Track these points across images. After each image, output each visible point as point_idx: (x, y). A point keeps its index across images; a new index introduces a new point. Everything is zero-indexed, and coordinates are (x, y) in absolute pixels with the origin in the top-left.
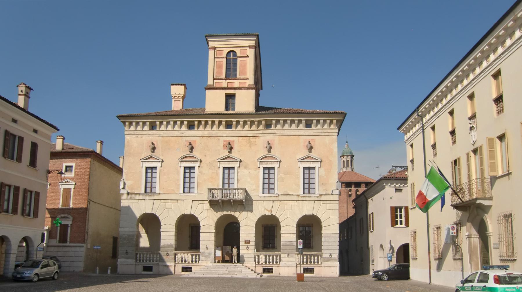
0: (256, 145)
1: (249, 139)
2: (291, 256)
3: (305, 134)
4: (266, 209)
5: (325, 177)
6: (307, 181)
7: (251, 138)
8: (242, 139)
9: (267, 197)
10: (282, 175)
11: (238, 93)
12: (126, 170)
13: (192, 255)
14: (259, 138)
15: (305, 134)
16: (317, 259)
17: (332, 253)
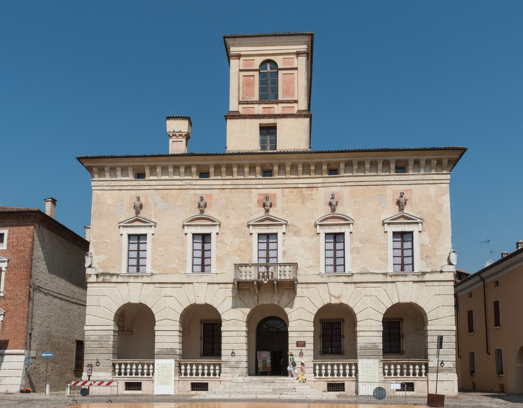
3: (394, 183)
7: (304, 189)
8: (290, 192)
10: (357, 244)
11: (280, 123)
14: (317, 190)
15: (394, 183)
16: (422, 369)
17: (444, 360)
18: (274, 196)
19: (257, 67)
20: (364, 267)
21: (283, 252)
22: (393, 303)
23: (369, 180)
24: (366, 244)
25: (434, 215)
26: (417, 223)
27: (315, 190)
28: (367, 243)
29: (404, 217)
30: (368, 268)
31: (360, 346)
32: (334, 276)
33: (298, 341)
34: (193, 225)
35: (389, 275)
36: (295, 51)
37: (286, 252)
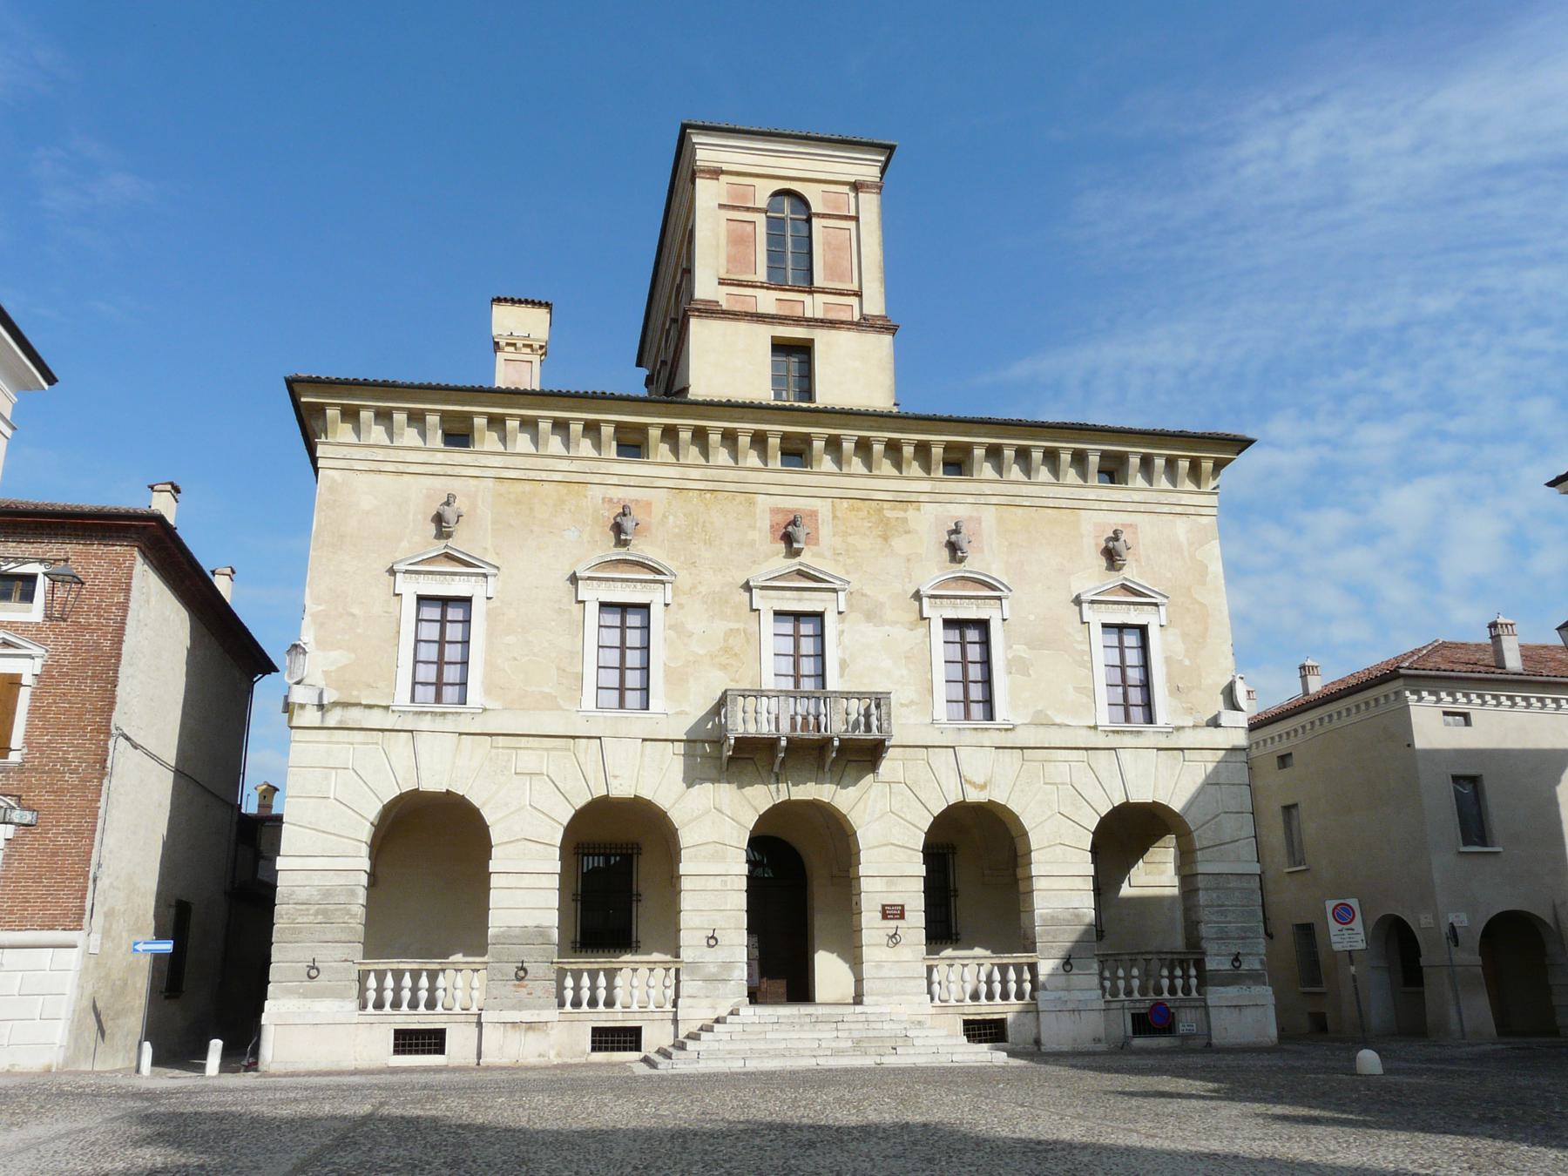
5: (1187, 662)
7: (886, 505)
8: (852, 509)
9: (968, 732)
10: (1020, 650)
19: (762, 201)
20: (1039, 708)
29: (801, 574)
30: (1049, 713)
31: (1041, 915)
33: (885, 903)
35: (1101, 731)
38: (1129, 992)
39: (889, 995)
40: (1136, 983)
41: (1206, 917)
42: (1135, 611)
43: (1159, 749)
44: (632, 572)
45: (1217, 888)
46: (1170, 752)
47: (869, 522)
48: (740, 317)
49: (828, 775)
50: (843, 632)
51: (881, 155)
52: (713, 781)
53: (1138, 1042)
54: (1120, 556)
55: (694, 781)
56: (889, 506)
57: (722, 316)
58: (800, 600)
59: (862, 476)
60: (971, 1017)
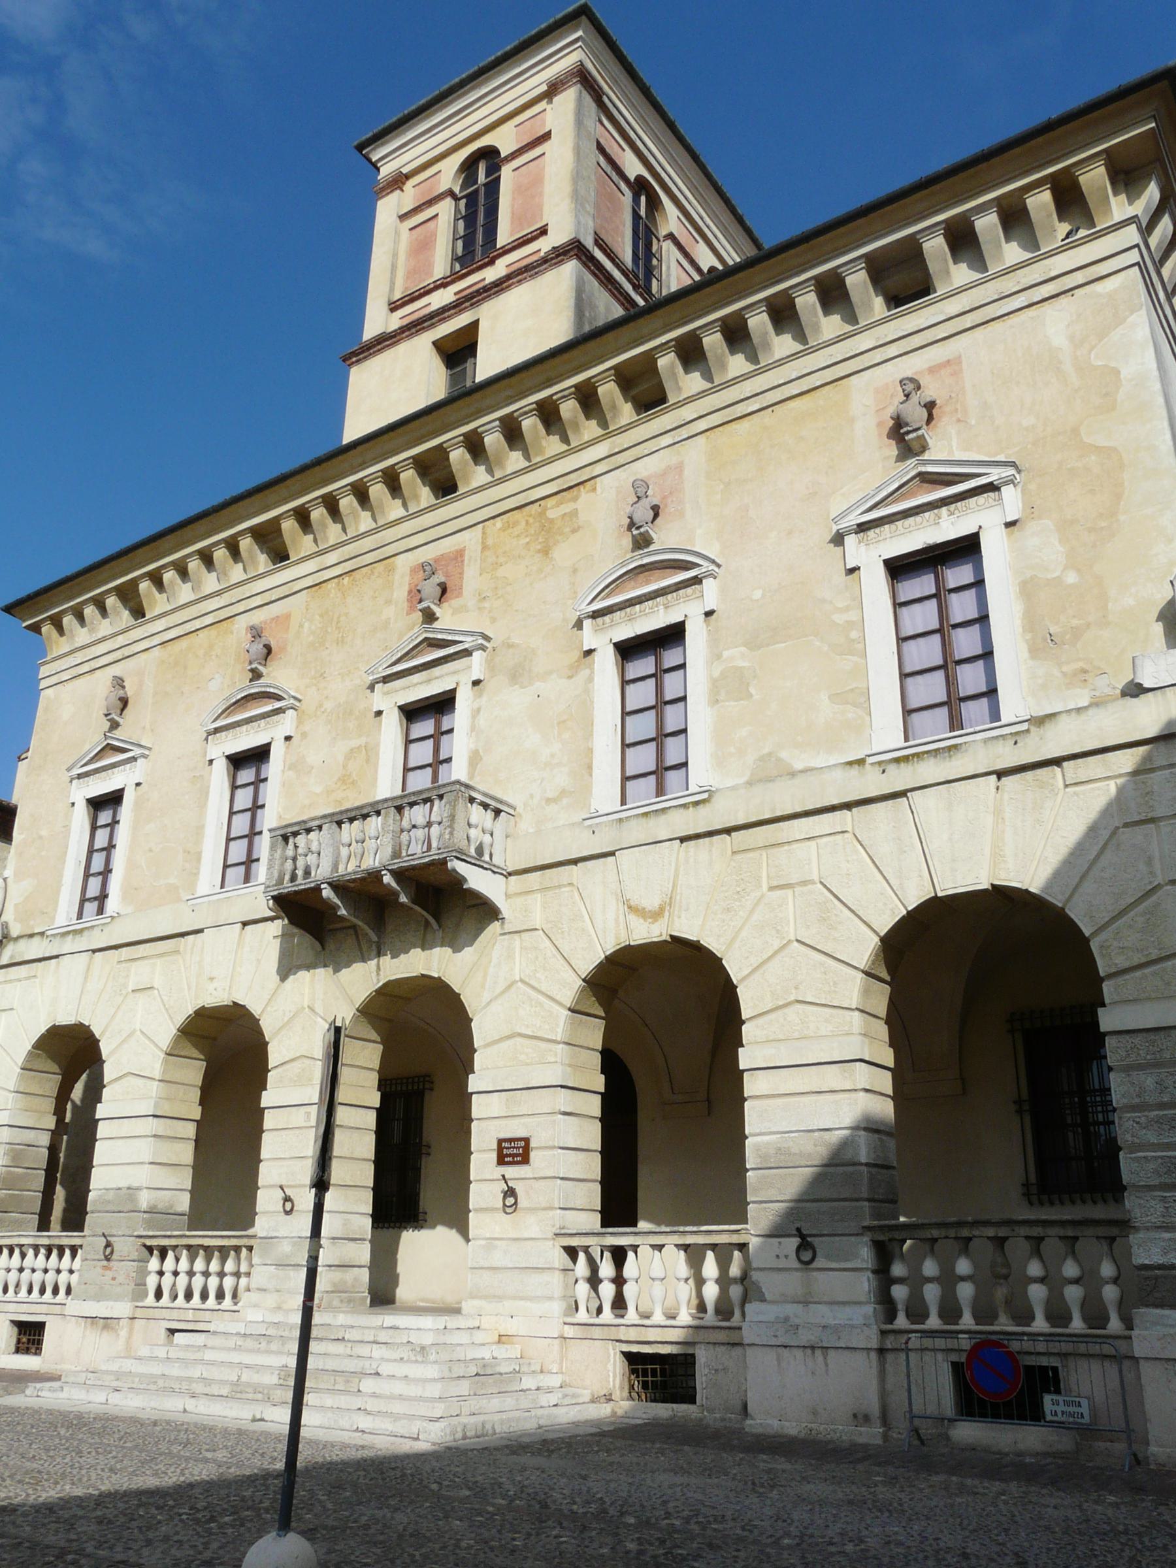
0: (574, 531)
1: (542, 514)
2: (828, 1257)
3: (878, 356)
4: (630, 907)
5: (1071, 578)
6: (966, 642)
7: (550, 502)
8: (507, 527)
9: (633, 822)
10: (736, 656)
12: (22, 834)
13: (694, 1255)
14: (594, 490)
15: (878, 356)
18: (456, 558)
20: (766, 751)
21: (470, 757)
22: (905, 907)
23: (776, 384)
24: (772, 647)
25: (1075, 431)
26: (992, 487)
27: (587, 492)
28: (777, 643)
29: (929, 480)
30: (784, 754)
31: (757, 1148)
32: (637, 816)
33: (503, 1136)
34: (633, 602)
35: (872, 764)
36: (544, 87)
37: (482, 754)
38: (950, 1312)
39: (499, 1298)
40: (965, 1291)
41: (1128, 1137)
42: (951, 514)
43: (1000, 774)
44: (648, 582)
45: (1157, 1065)
46: (1029, 775)
47: (527, 536)
48: (398, 338)
49: (440, 934)
50: (478, 710)
51: (576, 31)
52: (309, 967)
53: (968, 1432)
54: (907, 425)
55: (290, 970)
56: (554, 503)
57: (379, 347)
58: (429, 681)
59: (795, 356)
60: (635, 1349)
